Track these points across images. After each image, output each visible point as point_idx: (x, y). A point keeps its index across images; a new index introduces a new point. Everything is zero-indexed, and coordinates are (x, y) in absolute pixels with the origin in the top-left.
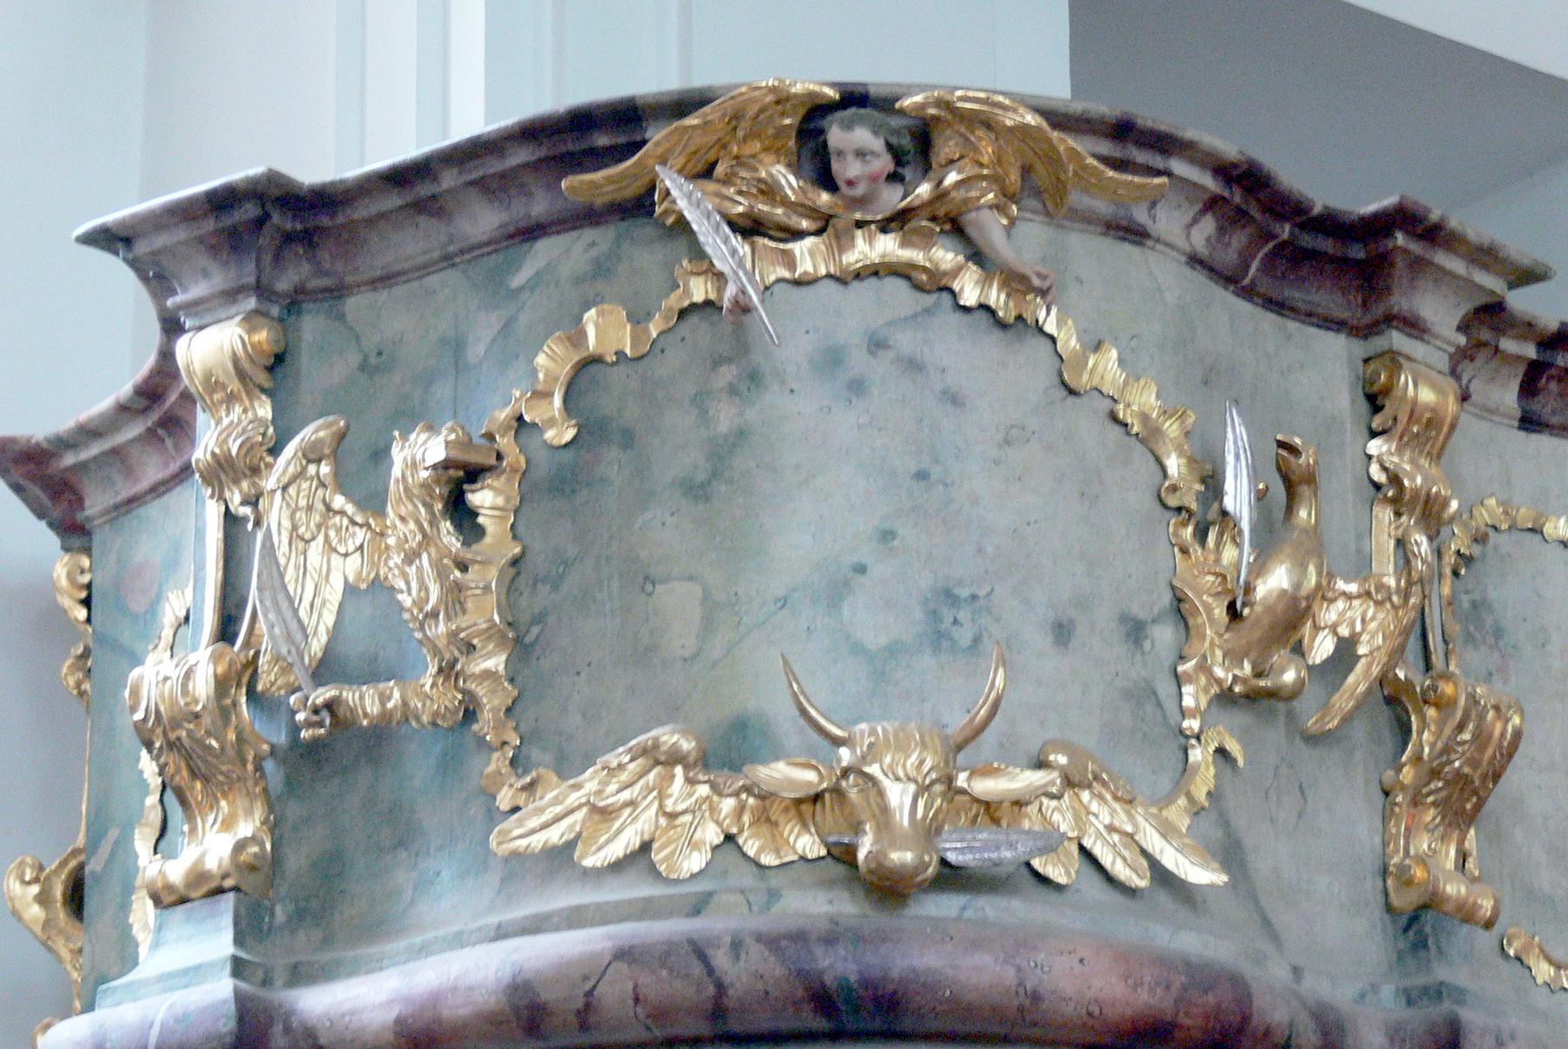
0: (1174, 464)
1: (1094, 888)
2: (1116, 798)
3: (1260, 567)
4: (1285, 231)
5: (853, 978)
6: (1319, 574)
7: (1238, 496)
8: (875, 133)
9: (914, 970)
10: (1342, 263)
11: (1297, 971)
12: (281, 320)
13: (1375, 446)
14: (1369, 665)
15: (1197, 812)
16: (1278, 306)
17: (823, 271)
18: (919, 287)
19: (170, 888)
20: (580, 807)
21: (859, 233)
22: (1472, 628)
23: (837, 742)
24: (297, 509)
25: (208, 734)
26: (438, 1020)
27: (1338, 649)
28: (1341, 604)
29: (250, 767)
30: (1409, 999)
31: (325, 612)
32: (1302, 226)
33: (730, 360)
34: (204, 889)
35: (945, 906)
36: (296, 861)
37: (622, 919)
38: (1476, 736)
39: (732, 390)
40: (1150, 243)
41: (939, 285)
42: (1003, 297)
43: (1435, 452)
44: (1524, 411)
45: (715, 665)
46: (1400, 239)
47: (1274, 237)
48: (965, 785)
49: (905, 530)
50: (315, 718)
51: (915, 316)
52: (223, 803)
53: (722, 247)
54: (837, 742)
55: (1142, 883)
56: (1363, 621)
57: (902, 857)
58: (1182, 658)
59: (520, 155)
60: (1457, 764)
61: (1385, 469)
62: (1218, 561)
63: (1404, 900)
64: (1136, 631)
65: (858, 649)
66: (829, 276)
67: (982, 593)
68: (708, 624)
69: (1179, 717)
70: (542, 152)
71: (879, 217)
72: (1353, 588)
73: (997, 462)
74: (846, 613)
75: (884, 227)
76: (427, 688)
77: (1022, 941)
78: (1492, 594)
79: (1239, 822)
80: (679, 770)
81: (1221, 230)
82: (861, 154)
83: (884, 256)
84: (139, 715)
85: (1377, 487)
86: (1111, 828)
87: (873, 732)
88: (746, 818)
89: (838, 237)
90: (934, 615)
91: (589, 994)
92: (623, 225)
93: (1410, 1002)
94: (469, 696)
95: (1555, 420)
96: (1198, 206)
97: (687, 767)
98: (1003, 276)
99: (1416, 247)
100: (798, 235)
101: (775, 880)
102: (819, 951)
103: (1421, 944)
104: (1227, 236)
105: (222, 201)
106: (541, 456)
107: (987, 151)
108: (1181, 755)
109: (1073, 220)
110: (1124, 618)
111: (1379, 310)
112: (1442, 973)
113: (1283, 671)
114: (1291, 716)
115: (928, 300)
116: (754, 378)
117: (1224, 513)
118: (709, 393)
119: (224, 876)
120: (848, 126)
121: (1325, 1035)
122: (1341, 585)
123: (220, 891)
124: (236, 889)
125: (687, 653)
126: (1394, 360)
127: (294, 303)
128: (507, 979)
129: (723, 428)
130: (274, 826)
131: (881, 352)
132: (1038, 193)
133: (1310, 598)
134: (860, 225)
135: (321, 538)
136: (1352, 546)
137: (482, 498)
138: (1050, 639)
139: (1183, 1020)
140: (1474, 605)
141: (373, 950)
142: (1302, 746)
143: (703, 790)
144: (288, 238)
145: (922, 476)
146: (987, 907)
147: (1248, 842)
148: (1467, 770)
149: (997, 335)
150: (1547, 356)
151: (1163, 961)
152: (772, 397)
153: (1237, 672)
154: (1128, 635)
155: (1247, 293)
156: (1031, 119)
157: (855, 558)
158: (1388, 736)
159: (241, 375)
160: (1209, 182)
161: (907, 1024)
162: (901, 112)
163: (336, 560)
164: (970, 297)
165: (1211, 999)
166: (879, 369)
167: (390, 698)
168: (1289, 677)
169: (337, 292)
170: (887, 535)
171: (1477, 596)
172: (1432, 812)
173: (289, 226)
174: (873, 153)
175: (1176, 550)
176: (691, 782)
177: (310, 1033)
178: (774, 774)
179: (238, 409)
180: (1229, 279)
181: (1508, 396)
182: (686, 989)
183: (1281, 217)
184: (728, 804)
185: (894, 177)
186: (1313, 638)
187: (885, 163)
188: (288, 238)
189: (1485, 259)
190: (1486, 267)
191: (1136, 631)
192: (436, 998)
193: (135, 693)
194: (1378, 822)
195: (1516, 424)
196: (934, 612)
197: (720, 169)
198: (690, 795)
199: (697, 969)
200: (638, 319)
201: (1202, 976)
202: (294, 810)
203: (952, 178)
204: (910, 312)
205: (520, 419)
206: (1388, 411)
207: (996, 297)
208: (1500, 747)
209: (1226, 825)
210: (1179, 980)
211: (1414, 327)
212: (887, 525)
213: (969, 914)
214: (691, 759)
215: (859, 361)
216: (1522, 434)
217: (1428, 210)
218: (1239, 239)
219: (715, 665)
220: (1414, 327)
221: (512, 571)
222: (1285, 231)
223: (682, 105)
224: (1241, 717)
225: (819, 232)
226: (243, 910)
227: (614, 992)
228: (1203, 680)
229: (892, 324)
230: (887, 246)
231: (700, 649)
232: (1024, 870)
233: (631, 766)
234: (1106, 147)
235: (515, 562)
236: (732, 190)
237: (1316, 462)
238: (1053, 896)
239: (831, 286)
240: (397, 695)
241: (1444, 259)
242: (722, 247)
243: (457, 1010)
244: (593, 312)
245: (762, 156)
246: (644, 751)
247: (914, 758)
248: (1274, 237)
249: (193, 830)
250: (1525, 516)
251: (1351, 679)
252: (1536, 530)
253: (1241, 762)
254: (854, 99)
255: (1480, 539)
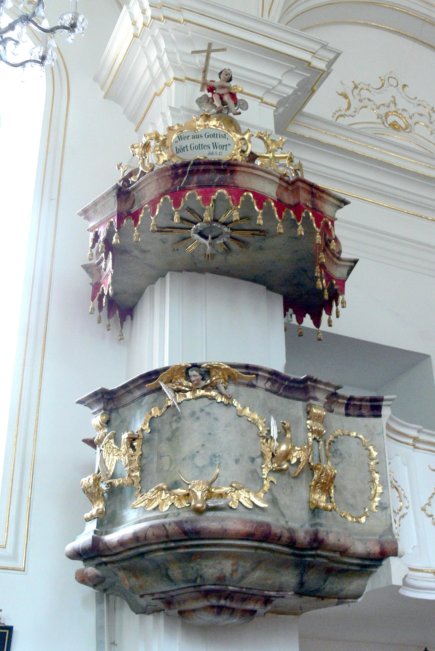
0: (261, 428)
1: (241, 509)
2: (246, 491)
3: (279, 447)
4: (287, 383)
5: (190, 528)
6: (291, 446)
7: (274, 433)
8: (197, 372)
9: (201, 526)
10: (299, 388)
11: (287, 522)
12: (109, 414)
13: (308, 422)
14: (303, 463)
15: (265, 493)
16: (287, 397)
17: (192, 398)
18: (210, 399)
19: (88, 518)
20: (146, 499)
21: (197, 390)
22: (334, 454)
23: (189, 484)
24: (107, 448)
25: (93, 490)
26: (123, 540)
27: (297, 460)
28: (297, 452)
29: (101, 495)
30: (312, 526)
31: (113, 466)
32: (290, 382)
33: (176, 415)
34: (93, 518)
35: (210, 514)
36: (109, 512)
37: (153, 520)
38: (326, 475)
39: (176, 421)
40: (256, 387)
41: (212, 398)
42: (225, 400)
43: (321, 421)
44: (346, 412)
45: (171, 472)
46: (309, 383)
47: (284, 384)
48: (213, 491)
49: (207, 445)
50: (108, 486)
51: (209, 405)
52: (97, 502)
53: (170, 394)
54: (189, 484)
55: (251, 507)
56: (301, 455)
57: (199, 505)
58: (263, 464)
59: (141, 381)
60: (322, 481)
61: (310, 426)
62: (270, 445)
63: (312, 507)
64: (253, 460)
65: (197, 467)
66: (193, 398)
67: (221, 454)
68: (171, 464)
69: (262, 475)
70: (144, 380)
71: (201, 387)
72: (299, 449)
73: (224, 430)
74: (195, 460)
75: (203, 389)
76: (127, 479)
77: (223, 519)
78: (339, 448)
79: (276, 494)
80: (164, 491)
81: (272, 384)
82: (194, 376)
83: (202, 394)
84: (82, 487)
85: (309, 429)
86: (245, 497)
87: (194, 482)
88: (176, 500)
89: (194, 391)
90: (211, 460)
91: (146, 534)
92: (159, 392)
93: (312, 527)
94: (133, 481)
95: (352, 414)
96: (266, 380)
97: (165, 491)
98: (154, 398)
99: (313, 384)
100: (187, 391)
101: (180, 511)
102: (184, 524)
103: (315, 515)
104: (268, 385)
105: (95, 394)
106: (145, 434)
107: (220, 374)
108: (262, 482)
109: (239, 384)
110: (250, 458)
111: (308, 397)
112: (318, 521)
113: (284, 465)
114: (289, 474)
115: (212, 401)
116: (180, 418)
117: (271, 437)
118: (172, 421)
119: (96, 516)
120: (192, 371)
121: (290, 533)
122: (296, 448)
123: (95, 518)
124: (97, 518)
125: (167, 470)
126: (310, 405)
127: (111, 411)
128: (133, 532)
129: (174, 428)
130: (106, 506)
131: (203, 412)
132: (232, 380)
133: (290, 451)
134: (198, 389)
135: (112, 453)
136: (303, 441)
137: (135, 444)
138: (234, 463)
139: (256, 533)
140: (335, 450)
141: (114, 529)
142: (292, 479)
143: (168, 495)
144: (109, 399)
145: (210, 434)
146: (219, 514)
147: (278, 498)
148: (325, 481)
149: (225, 407)
150: (349, 402)
151: (252, 522)
152: (183, 421)
153: (274, 466)
154: (251, 461)
155: (280, 395)
156: (227, 367)
157: (196, 450)
158: (311, 475)
159: (101, 425)
160: (267, 375)
161: (202, 536)
162: (203, 368)
163: (115, 457)
164: (219, 400)
165: (262, 528)
166: (203, 414)
167: (120, 481)
168: (285, 466)
169: (117, 409)
170: (203, 445)
171: (336, 448)
172: (319, 490)
173: (108, 397)
174: (197, 376)
175: (262, 444)
176: (166, 493)
177: (106, 543)
178: (178, 491)
179: (102, 431)
180: (275, 393)
181: (343, 410)
182: (161, 532)
183: (285, 381)
184: (173, 497)
185: (203, 379)
186: (292, 458)
187: (200, 377)
188: (109, 399)
189: (328, 385)
190: (329, 387)
191: (253, 460)
192: (123, 536)
193: (82, 483)
194: (308, 493)
195: (344, 415)
196: (212, 459)
197: (173, 381)
198: (166, 496)
199: (163, 529)
200: (160, 409)
201: (261, 524)
202: (109, 503)
203: (214, 378)
204: (208, 404)
205: (142, 429)
206: (310, 415)
207: (223, 400)
208: (331, 477)
209: (273, 495)
210: (255, 526)
211: (315, 399)
212: (203, 443)
213: (215, 515)
214: (165, 489)
215: (198, 414)
216: (346, 417)
217: (291, 377)
218: (277, 385)
219: (171, 472)
220: (315, 399)
221: (140, 457)
222: (287, 383)
223: (165, 369)
224: (277, 475)
225: (190, 391)
226: (99, 522)
227: (150, 534)
228: (267, 469)
229: (204, 406)
230: (202, 392)
231: (169, 469)
232: (228, 506)
233: (155, 491)
234: (244, 371)
235: (141, 455)
236: (174, 384)
237: (289, 425)
238: (233, 511)
239: (194, 401)
240: (121, 481)
241: (319, 386)
242: (170, 394)
243: (126, 538)
244: (153, 409)
245: (180, 378)
246: (157, 488)
247: (201, 487)
248: (284, 384)
249: (94, 507)
250: (346, 433)
251: (300, 466)
252: (349, 435)
253: (276, 483)
254: (195, 366)
255: (336, 437)
